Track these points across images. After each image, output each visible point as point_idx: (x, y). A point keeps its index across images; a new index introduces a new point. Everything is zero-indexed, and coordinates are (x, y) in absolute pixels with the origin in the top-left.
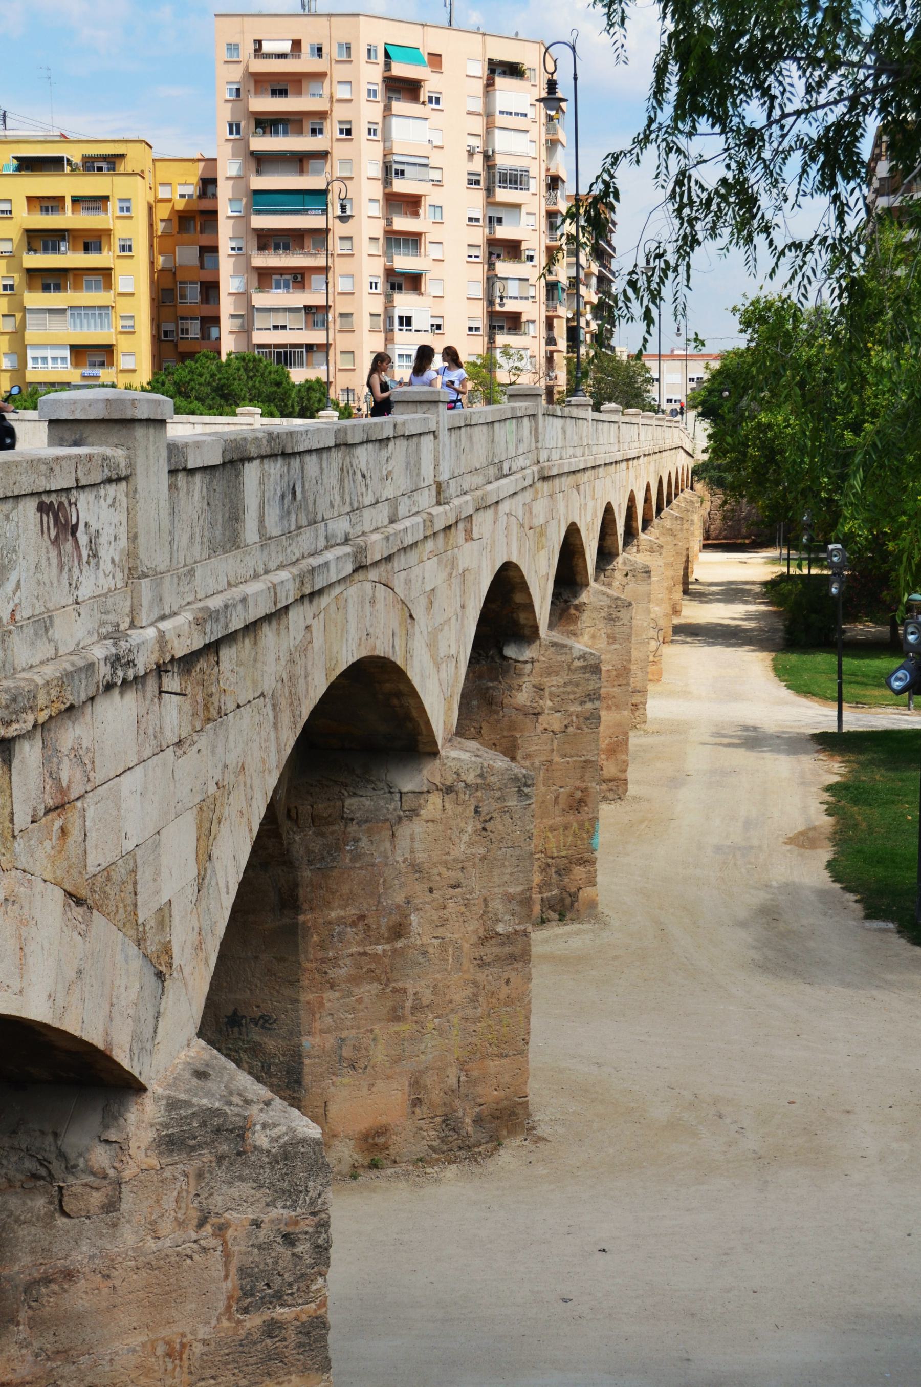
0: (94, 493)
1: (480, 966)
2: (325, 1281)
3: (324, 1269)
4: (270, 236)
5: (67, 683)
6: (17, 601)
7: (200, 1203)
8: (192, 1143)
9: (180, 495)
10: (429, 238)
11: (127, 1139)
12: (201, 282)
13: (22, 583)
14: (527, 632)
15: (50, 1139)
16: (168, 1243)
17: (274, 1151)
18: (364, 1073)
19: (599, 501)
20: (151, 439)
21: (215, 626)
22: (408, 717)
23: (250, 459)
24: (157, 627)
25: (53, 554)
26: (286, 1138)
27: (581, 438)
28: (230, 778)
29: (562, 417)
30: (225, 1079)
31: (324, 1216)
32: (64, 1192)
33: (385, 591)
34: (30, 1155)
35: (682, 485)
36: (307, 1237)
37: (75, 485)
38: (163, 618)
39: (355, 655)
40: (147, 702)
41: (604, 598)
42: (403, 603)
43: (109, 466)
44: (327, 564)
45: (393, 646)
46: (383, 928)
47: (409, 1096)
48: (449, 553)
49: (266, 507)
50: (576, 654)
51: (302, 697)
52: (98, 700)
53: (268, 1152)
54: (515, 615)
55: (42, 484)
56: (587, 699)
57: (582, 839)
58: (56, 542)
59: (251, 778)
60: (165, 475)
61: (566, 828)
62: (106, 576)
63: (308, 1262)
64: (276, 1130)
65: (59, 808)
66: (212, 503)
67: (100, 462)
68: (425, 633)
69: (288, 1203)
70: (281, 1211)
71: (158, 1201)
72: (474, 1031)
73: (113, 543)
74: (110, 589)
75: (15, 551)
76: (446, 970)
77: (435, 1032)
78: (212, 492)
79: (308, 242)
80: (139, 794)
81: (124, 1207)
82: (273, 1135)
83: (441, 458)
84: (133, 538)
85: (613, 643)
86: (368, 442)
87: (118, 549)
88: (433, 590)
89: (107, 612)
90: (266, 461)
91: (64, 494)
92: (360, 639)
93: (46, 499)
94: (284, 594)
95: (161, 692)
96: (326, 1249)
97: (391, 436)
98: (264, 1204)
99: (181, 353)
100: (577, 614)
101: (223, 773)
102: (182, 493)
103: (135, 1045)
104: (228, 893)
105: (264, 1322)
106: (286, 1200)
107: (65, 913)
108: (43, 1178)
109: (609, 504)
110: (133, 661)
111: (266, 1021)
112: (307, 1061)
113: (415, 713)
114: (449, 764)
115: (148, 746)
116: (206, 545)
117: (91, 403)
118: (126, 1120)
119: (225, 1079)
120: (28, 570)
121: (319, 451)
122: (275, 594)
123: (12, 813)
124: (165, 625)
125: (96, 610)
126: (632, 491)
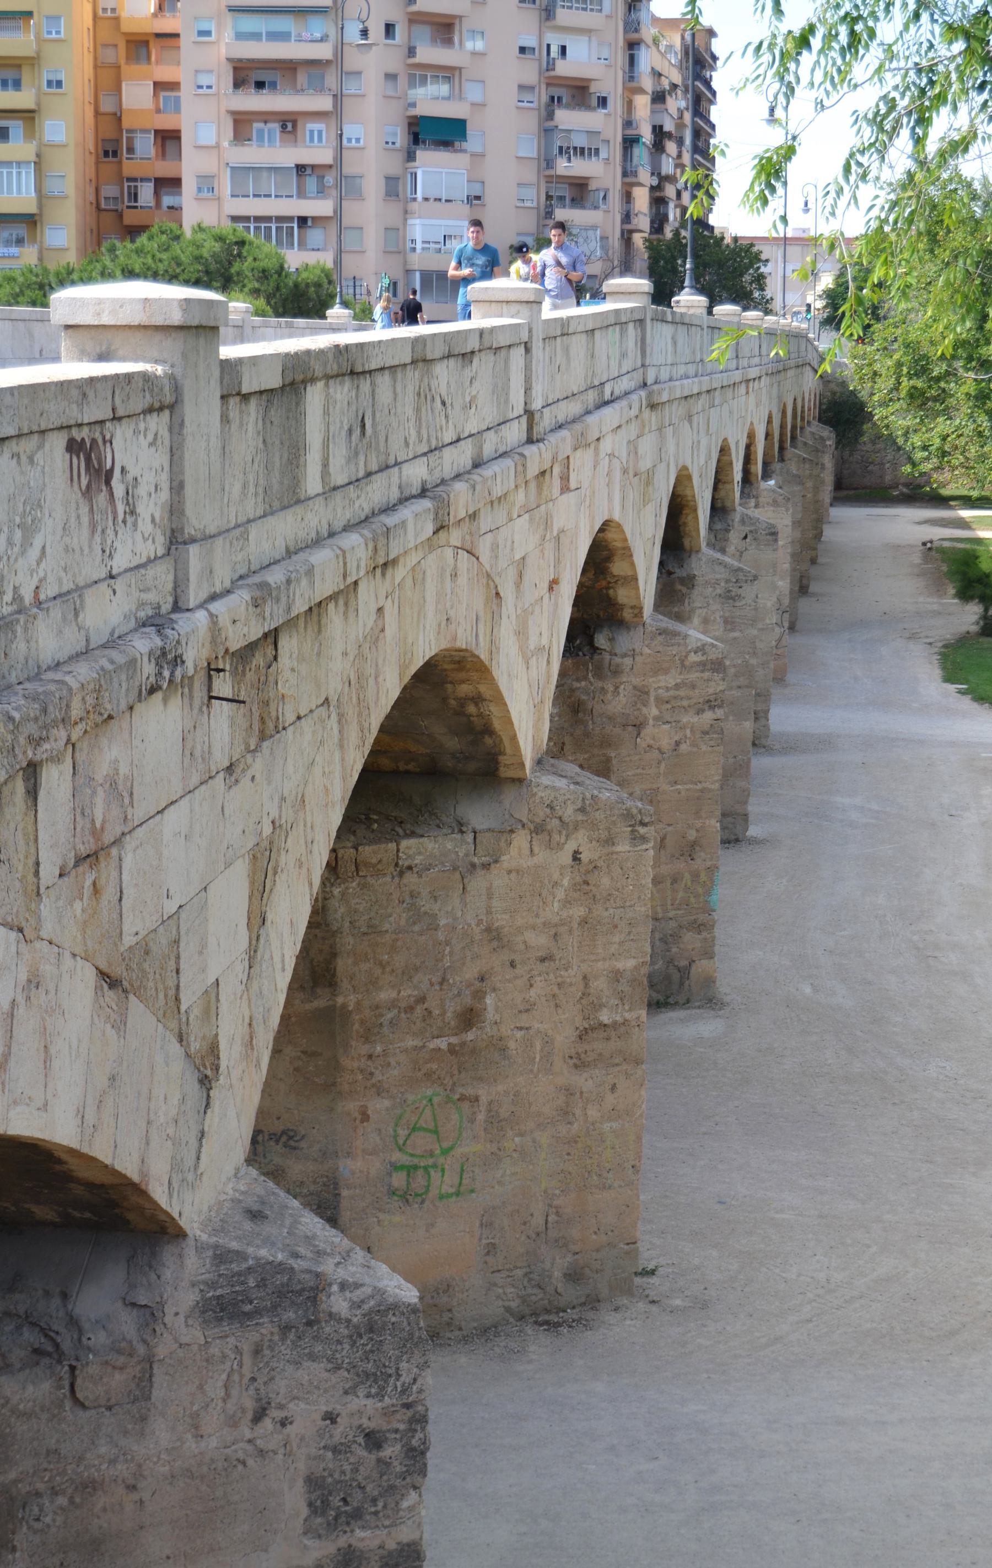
0: (133, 426)
1: (576, 1066)
2: (420, 1495)
3: (419, 1479)
4: (250, 69)
5: (104, 687)
6: (41, 574)
7: (257, 1390)
8: (247, 1308)
9: (232, 430)
10: (466, 25)
11: (162, 1304)
12: (156, 132)
13: (48, 549)
14: (627, 615)
15: (56, 1301)
16: (214, 1443)
17: (355, 1320)
18: (420, 1208)
19: (714, 437)
20: (202, 353)
21: (275, 607)
22: (488, 730)
23: (313, 380)
24: (207, 610)
25: (84, 510)
26: (372, 1303)
27: (694, 352)
28: (288, 815)
29: (672, 322)
30: (288, 1222)
31: (420, 1408)
32: (77, 1372)
33: (469, 559)
34: (31, 1323)
35: (809, 415)
36: (398, 1436)
37: (112, 416)
38: (214, 597)
39: (433, 647)
40: (196, 711)
41: (721, 569)
42: (488, 576)
43: (151, 391)
44: (404, 523)
45: (477, 635)
46: (449, 1014)
47: (480, 1239)
48: (543, 508)
49: (331, 446)
50: (692, 644)
51: (372, 705)
52: (139, 707)
53: (348, 1321)
54: (611, 592)
55: (74, 414)
56: (706, 707)
57: (697, 896)
58: (88, 493)
59: (312, 814)
60: (217, 402)
61: (675, 881)
62: (145, 540)
63: (398, 1469)
64: (358, 1292)
65: (90, 858)
66: (269, 441)
67: (140, 384)
68: (513, 617)
69: (373, 1391)
70: (364, 1402)
71: (201, 1387)
72: (568, 1154)
73: (153, 495)
74: (149, 557)
75: (40, 506)
76: (532, 1071)
77: (515, 1155)
78: (269, 425)
79: (302, 78)
80: (183, 837)
81: (156, 1393)
82: (355, 1299)
83: (534, 378)
84: (177, 488)
85: (732, 630)
86: (449, 356)
87: (160, 503)
88: (523, 558)
89: (146, 590)
90: (331, 382)
91: (98, 428)
92: (439, 625)
93: (77, 434)
94: (355, 565)
95: (211, 698)
96: (423, 1453)
97: (477, 349)
98: (341, 1392)
99: (127, 226)
100: (684, 590)
101: (280, 807)
102: (234, 427)
103: (174, 1175)
104: (283, 970)
105: (339, 1550)
106: (370, 1386)
107: (96, 1000)
108: (49, 1355)
109: (725, 440)
110: (181, 656)
111: (291, 1138)
112: (345, 1193)
113: (497, 725)
114: (540, 794)
115: (194, 771)
116: (260, 498)
117: (122, 303)
118: (159, 1277)
119: (288, 1222)
120: (54, 533)
121: (393, 368)
122: (345, 564)
123: (38, 864)
124: (215, 607)
125: (133, 586)
126: (752, 424)
